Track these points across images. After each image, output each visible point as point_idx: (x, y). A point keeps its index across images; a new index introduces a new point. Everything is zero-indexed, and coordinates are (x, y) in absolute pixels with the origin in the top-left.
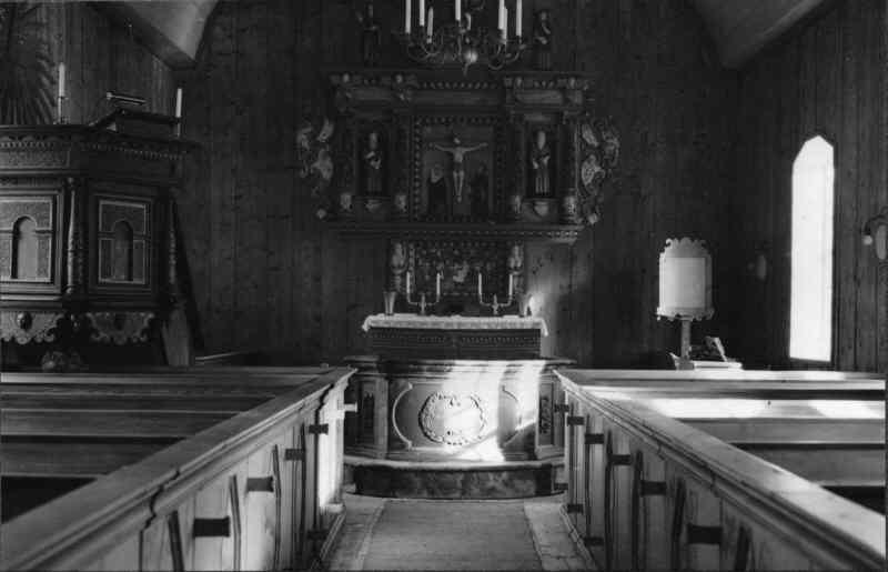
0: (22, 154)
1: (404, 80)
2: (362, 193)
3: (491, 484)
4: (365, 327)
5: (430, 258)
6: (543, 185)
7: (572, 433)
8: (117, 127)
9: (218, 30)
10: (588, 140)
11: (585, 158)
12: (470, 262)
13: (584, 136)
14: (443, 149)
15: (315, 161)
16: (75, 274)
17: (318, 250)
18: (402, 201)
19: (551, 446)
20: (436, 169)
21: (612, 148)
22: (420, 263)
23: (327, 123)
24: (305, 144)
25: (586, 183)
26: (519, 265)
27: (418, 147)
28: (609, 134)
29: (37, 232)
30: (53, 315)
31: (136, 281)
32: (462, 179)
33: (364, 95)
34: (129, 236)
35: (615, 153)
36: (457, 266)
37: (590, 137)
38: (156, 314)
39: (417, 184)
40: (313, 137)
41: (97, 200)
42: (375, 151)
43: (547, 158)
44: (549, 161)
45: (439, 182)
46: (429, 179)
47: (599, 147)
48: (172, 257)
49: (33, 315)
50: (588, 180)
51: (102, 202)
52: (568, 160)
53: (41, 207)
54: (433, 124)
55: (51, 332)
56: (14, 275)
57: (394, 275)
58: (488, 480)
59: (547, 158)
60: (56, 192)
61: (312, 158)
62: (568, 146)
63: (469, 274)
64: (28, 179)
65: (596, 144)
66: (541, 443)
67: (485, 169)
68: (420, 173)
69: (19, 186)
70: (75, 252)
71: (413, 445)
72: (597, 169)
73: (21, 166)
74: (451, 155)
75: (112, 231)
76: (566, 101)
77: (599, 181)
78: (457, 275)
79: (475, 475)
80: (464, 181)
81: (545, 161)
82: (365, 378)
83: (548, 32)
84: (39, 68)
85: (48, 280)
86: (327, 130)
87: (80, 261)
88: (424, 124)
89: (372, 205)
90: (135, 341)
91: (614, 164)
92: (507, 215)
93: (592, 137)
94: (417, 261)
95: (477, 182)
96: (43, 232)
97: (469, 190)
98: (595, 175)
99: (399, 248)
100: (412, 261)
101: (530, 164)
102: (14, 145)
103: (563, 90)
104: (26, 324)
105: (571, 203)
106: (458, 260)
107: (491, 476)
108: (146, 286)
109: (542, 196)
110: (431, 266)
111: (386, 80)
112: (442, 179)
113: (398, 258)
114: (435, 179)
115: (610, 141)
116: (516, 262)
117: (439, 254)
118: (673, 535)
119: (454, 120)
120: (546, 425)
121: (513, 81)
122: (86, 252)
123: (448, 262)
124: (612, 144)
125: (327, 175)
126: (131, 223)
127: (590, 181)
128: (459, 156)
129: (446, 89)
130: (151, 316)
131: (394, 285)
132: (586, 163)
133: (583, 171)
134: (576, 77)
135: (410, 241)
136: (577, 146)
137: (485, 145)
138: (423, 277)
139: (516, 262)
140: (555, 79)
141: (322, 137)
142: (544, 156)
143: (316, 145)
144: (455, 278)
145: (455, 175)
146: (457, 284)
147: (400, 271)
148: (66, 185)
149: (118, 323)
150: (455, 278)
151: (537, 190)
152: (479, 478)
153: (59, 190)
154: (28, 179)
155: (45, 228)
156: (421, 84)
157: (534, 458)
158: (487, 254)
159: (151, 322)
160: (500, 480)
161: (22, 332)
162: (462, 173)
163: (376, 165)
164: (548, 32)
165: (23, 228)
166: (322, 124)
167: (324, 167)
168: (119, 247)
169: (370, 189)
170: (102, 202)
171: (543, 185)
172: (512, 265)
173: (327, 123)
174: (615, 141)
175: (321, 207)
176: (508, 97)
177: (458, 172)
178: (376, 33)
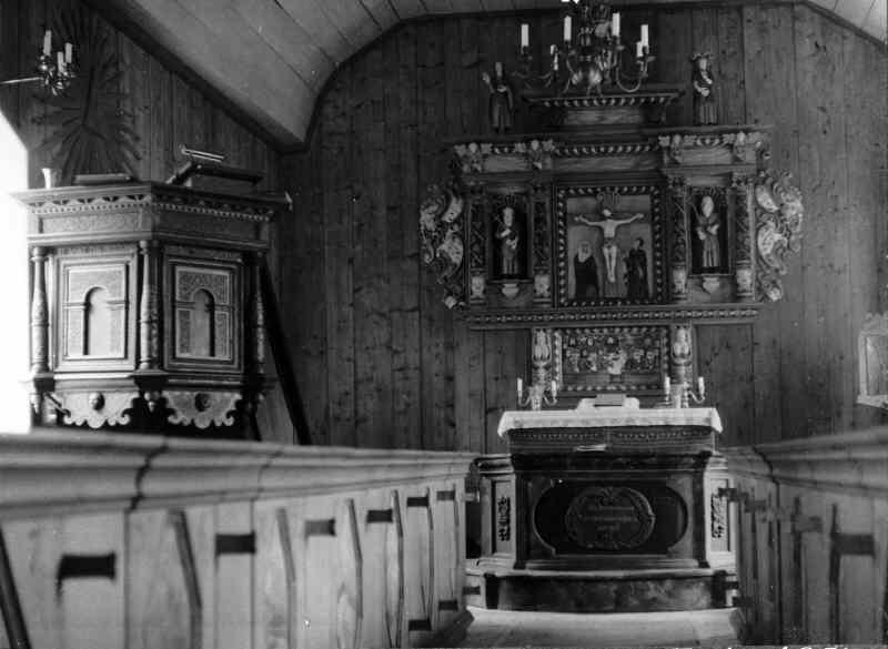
0: (91, 218)
1: (541, 146)
2: (496, 277)
3: (651, 594)
4: (501, 430)
5: (582, 348)
6: (711, 258)
7: (513, 270)
8: (193, 183)
9: (328, 110)
10: (765, 205)
11: (760, 226)
12: (628, 349)
13: (760, 200)
14: (590, 223)
15: (441, 242)
16: (150, 349)
17: (450, 347)
18: (543, 283)
19: (727, 553)
20: (584, 246)
21: (794, 213)
22: (568, 354)
23: (454, 200)
24: (431, 225)
25: (764, 254)
26: (686, 351)
27: (561, 223)
28: (788, 196)
29: (110, 303)
30: (127, 394)
31: (220, 356)
32: (614, 256)
33: (494, 165)
34: (211, 308)
35: (798, 219)
36: (612, 355)
37: (766, 200)
38: (243, 393)
39: (562, 264)
40: (438, 217)
41: (173, 266)
42: (510, 228)
43: (716, 227)
44: (718, 230)
45: (587, 261)
46: (577, 257)
47: (780, 213)
48: (260, 322)
49: (105, 395)
50: (766, 250)
51: (179, 269)
52: (740, 228)
53: (112, 276)
54: (578, 195)
55: (126, 412)
56: (86, 352)
57: (537, 368)
58: (649, 589)
59: (716, 227)
60: (128, 258)
61: (436, 242)
62: (741, 213)
63: (627, 364)
64: (101, 245)
65: (775, 208)
66: (714, 548)
67: (642, 243)
68: (565, 251)
69: (90, 254)
70: (150, 322)
71: (557, 552)
72: (777, 237)
73: (90, 231)
74: (601, 230)
75: (191, 300)
76: (736, 160)
77: (780, 251)
78: (612, 366)
79: (632, 584)
80: (617, 258)
81: (714, 230)
82: (498, 478)
83: (710, 82)
84: (121, 142)
85: (122, 355)
86: (455, 208)
87: (154, 332)
88: (568, 195)
89: (510, 289)
90: (218, 424)
91: (798, 229)
92: (668, 295)
93: (770, 201)
94: (564, 351)
95: (634, 259)
96: (115, 302)
97: (624, 270)
98: (775, 244)
99: (541, 336)
100: (558, 352)
101: (694, 235)
102: (83, 210)
103: (731, 147)
104: (100, 404)
105: (746, 277)
106: (613, 348)
107: (651, 585)
108: (232, 362)
109: (712, 270)
110: (582, 356)
111: (520, 147)
112: (591, 258)
113: (541, 349)
114: (583, 258)
115: (790, 204)
116: (683, 349)
117: (590, 343)
118: (795, 559)
119: (603, 189)
120: (720, 528)
121: (671, 141)
122: (161, 323)
123: (601, 353)
124: (793, 208)
125: (456, 259)
126: (212, 291)
127: (769, 251)
128: (610, 229)
129: (591, 155)
130: (238, 396)
131: (538, 379)
132: (762, 231)
133: (760, 240)
134: (746, 132)
135: (556, 329)
136: (750, 210)
137: (641, 216)
138: (572, 370)
139: (683, 349)
140: (720, 134)
141: (447, 218)
142: (713, 225)
143: (442, 226)
144: (610, 370)
145: (606, 251)
146: (612, 376)
147: (543, 364)
148: (140, 249)
149: (200, 405)
150: (610, 370)
151: (705, 265)
152: (636, 588)
153: (133, 255)
154: (101, 245)
155: (117, 299)
156: (562, 149)
157: (705, 565)
158: (648, 341)
159: (238, 403)
160: (663, 591)
161: (95, 413)
162: (614, 249)
163: (513, 244)
164: (710, 82)
165: (94, 300)
166: (448, 200)
167: (453, 249)
168: (200, 320)
169: (505, 272)
170: (179, 269)
171: (711, 258)
172: (678, 351)
173: (454, 200)
174: (798, 204)
175: (450, 293)
176: (666, 159)
177: (609, 247)
178: (505, 94)
